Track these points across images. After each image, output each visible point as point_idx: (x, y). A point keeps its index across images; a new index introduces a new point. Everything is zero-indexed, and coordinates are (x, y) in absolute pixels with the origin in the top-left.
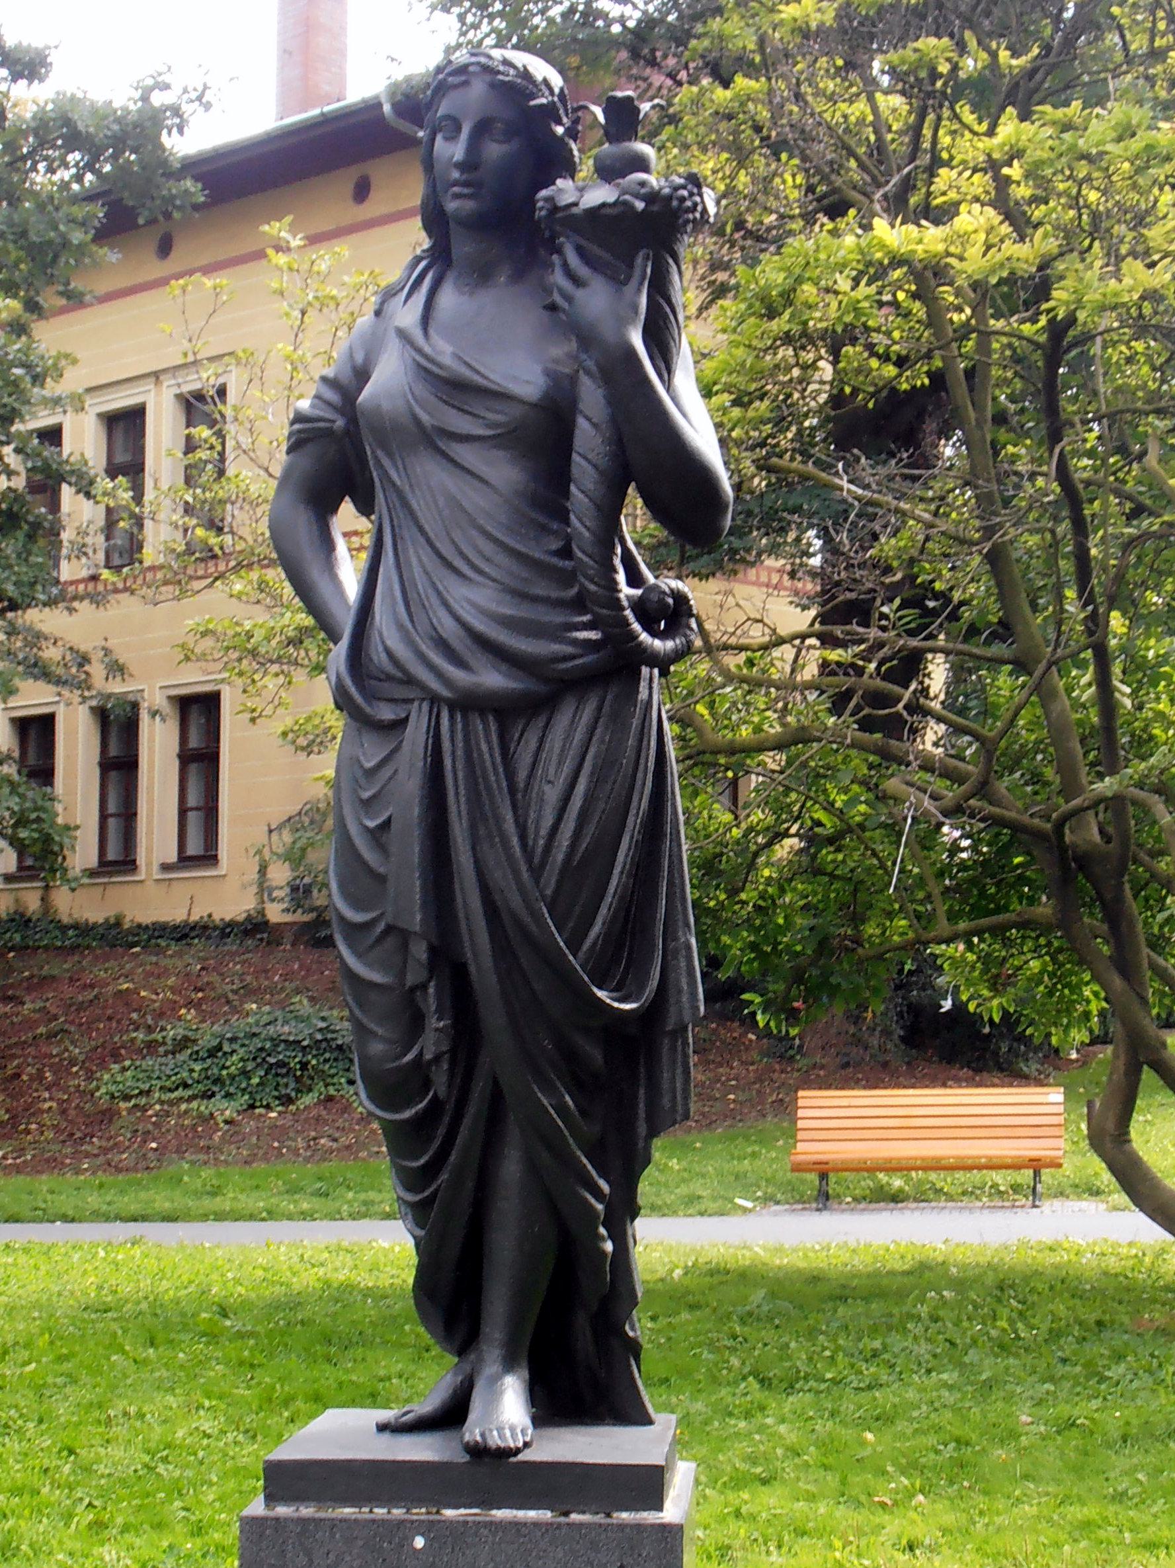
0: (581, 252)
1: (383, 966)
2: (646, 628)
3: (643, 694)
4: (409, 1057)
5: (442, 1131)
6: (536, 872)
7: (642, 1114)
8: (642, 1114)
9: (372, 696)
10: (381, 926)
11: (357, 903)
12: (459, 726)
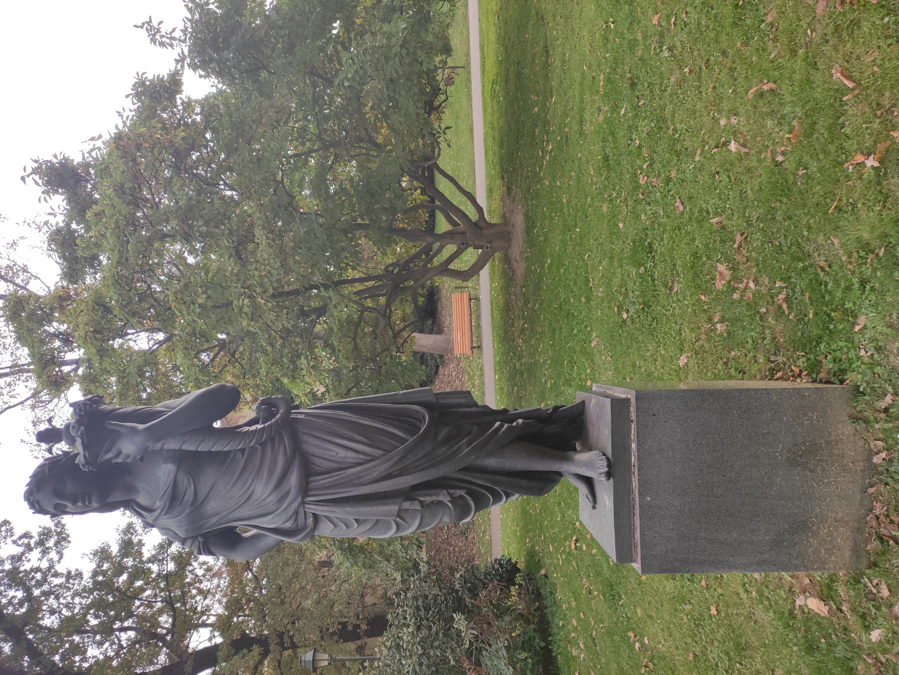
0: (107, 452)
1: (413, 518)
2: (274, 416)
3: (302, 416)
4: (450, 505)
5: (478, 489)
6: (373, 458)
7: (467, 410)
8: (467, 410)
9: (305, 527)
10: (398, 519)
11: (390, 528)
12: (314, 493)
